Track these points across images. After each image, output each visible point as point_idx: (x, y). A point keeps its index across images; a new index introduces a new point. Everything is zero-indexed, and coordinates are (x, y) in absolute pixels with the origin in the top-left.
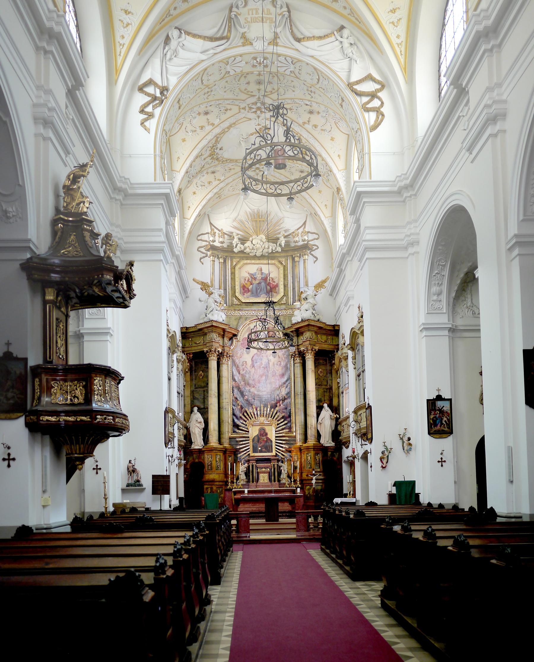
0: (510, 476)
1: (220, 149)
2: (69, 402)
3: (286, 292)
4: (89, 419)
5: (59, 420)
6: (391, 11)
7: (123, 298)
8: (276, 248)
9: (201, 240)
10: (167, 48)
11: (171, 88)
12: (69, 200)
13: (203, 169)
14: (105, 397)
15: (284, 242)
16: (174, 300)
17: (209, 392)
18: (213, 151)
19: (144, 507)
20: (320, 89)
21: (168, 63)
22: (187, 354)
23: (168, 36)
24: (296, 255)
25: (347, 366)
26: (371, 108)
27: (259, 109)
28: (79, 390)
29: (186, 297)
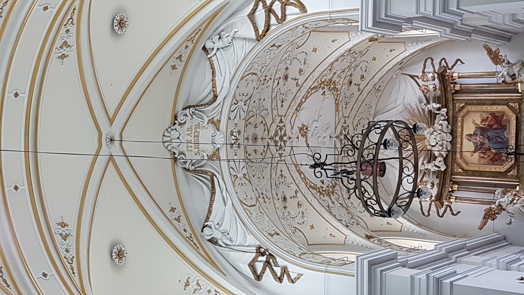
1: (323, 183)
3: (503, 102)
8: (443, 115)
9: (429, 211)
10: (221, 243)
11: (258, 243)
13: (344, 205)
15: (434, 104)
16: (508, 263)
18: (324, 192)
20: (262, 71)
21: (234, 243)
23: (209, 240)
24: (452, 88)
27: (281, 138)
29: (505, 239)
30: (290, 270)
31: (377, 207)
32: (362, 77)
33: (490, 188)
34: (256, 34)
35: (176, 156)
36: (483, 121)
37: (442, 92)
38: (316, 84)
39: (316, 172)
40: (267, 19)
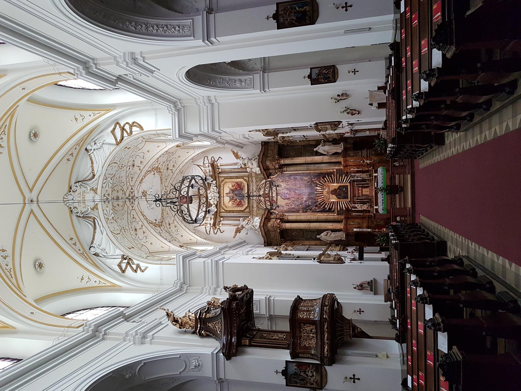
0: (366, 31)
2: (314, 335)
3: (241, 177)
4: (326, 323)
5: (327, 343)
6: (76, 121)
7: (247, 294)
8: (214, 184)
9: (210, 232)
10: (101, 255)
11: (122, 253)
12: (188, 326)
13: (168, 231)
14: (311, 311)
17: (306, 228)
19: (388, 281)
20: (120, 161)
21: (109, 255)
22: (281, 243)
25: (288, 137)
26: (130, 131)
27: (132, 198)
28: (306, 328)
30: (141, 265)
31: (189, 219)
32: (174, 166)
33: (237, 218)
34: (116, 141)
35: (72, 209)
36: (233, 186)
37: (213, 173)
38: (150, 169)
39: (157, 204)
40: (122, 133)
